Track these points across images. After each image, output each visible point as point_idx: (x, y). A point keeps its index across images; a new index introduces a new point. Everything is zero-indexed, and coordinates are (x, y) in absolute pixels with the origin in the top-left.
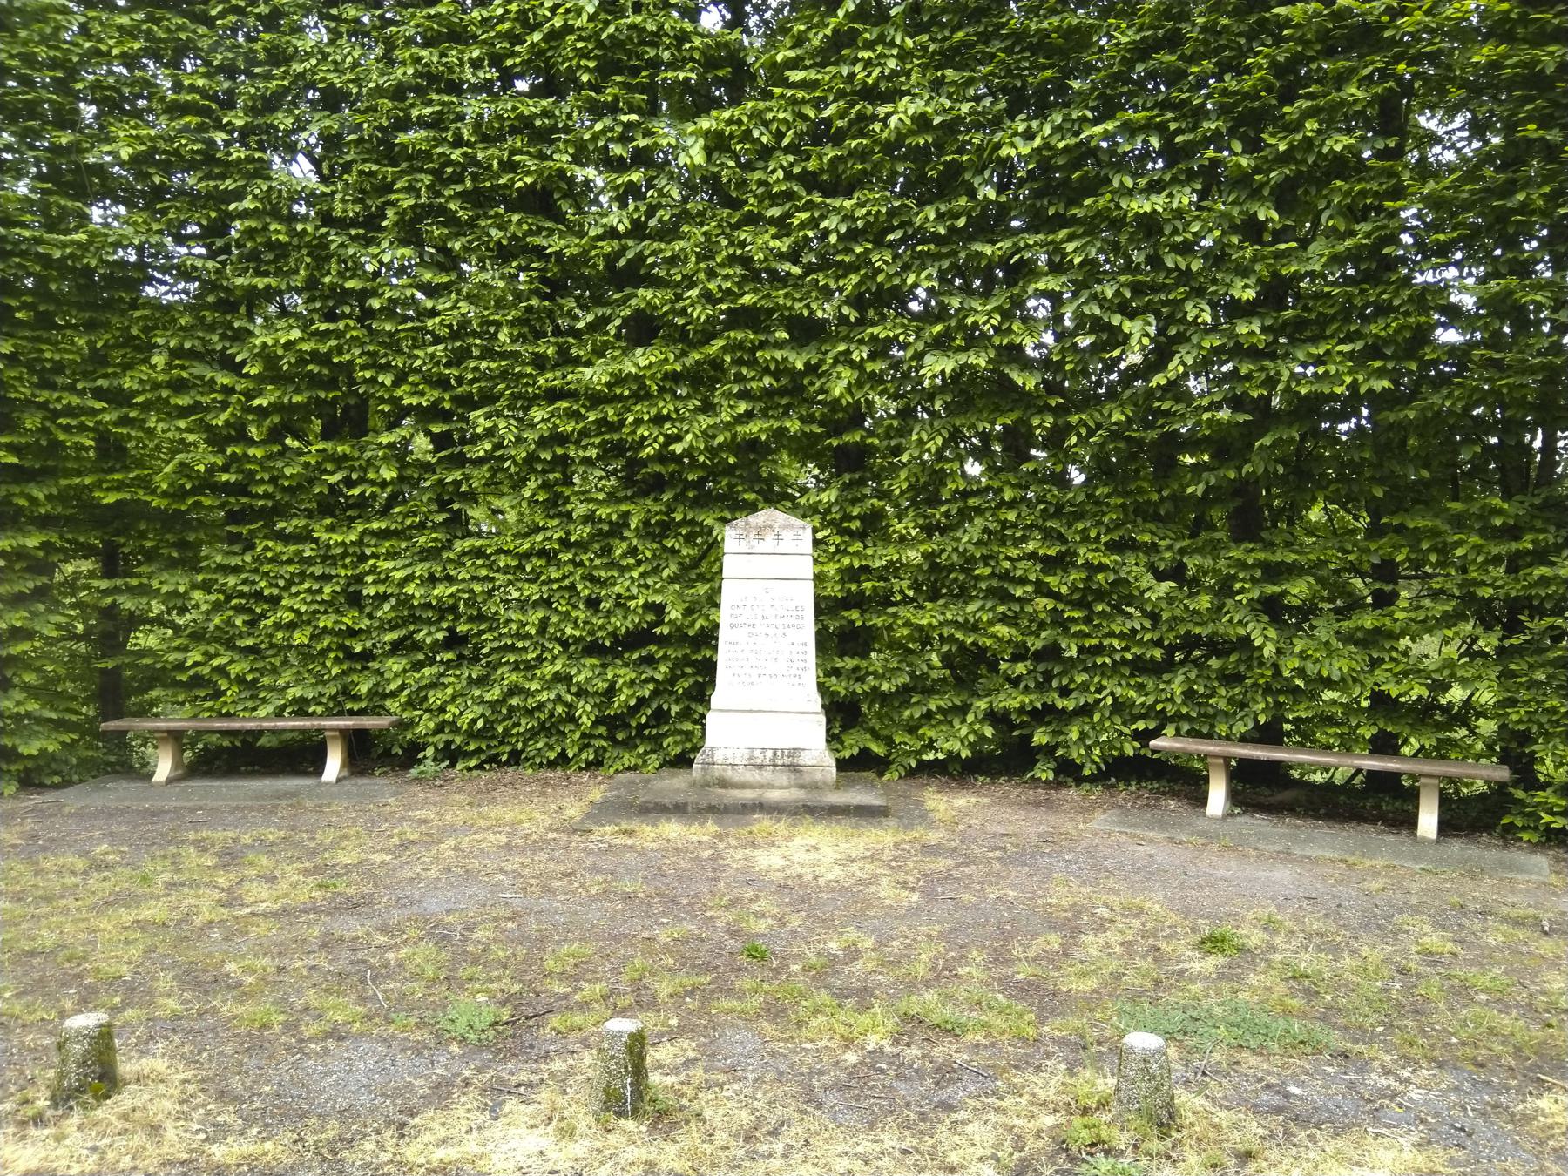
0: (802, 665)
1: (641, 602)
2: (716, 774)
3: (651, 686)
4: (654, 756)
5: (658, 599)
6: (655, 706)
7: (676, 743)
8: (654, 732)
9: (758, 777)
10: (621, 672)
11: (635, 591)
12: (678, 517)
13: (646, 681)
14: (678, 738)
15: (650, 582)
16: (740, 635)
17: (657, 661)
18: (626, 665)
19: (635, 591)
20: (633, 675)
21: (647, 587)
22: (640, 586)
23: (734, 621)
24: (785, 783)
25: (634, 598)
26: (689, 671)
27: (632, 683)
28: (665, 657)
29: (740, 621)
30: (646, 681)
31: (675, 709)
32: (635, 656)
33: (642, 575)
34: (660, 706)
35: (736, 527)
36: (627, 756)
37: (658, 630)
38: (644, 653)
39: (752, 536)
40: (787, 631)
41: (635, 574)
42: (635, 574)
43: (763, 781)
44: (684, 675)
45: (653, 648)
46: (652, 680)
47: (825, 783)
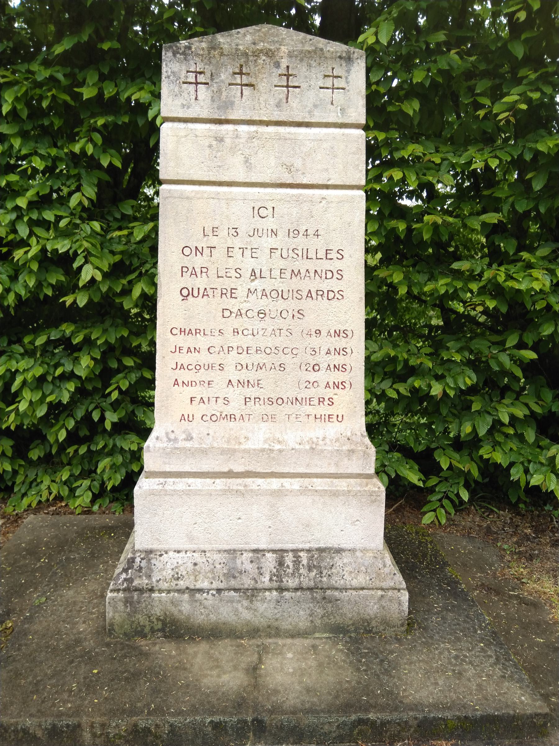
0: (338, 376)
1: (34, 250)
2: (157, 611)
3: (71, 386)
4: (86, 483)
5: (63, 246)
6: (80, 413)
7: (114, 468)
8: (83, 450)
9: (246, 615)
10: (23, 365)
11: (23, 231)
12: (88, 93)
13: (65, 377)
14: (119, 459)
15: (49, 216)
16: (360, 284)
17: (78, 348)
18: (29, 353)
19: (23, 231)
20: (39, 371)
21: (45, 224)
22: (32, 223)
23: (189, 282)
24: (303, 624)
25: (24, 243)
26: (129, 362)
27: (41, 380)
28: (88, 342)
29: (200, 282)
30: (65, 377)
31: (111, 418)
32: (40, 341)
33: (31, 205)
34: (88, 416)
35: (186, 53)
36: (47, 481)
37: (69, 300)
38: (55, 335)
39: (224, 76)
40: (307, 304)
41: (22, 202)
42: (22, 202)
43: (258, 621)
44: (122, 368)
45: (67, 329)
46: (70, 376)
47: (386, 622)
